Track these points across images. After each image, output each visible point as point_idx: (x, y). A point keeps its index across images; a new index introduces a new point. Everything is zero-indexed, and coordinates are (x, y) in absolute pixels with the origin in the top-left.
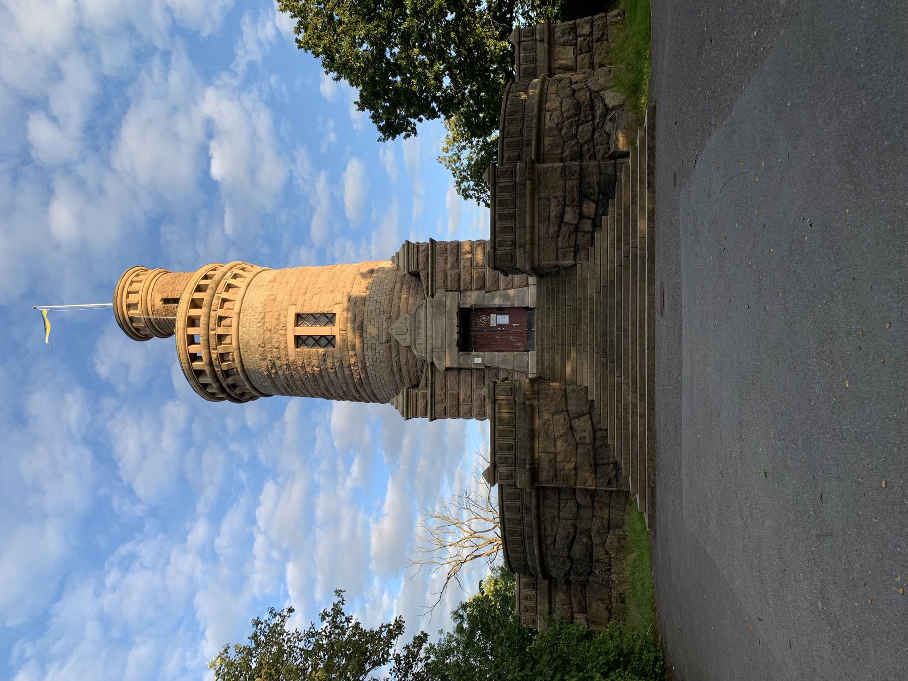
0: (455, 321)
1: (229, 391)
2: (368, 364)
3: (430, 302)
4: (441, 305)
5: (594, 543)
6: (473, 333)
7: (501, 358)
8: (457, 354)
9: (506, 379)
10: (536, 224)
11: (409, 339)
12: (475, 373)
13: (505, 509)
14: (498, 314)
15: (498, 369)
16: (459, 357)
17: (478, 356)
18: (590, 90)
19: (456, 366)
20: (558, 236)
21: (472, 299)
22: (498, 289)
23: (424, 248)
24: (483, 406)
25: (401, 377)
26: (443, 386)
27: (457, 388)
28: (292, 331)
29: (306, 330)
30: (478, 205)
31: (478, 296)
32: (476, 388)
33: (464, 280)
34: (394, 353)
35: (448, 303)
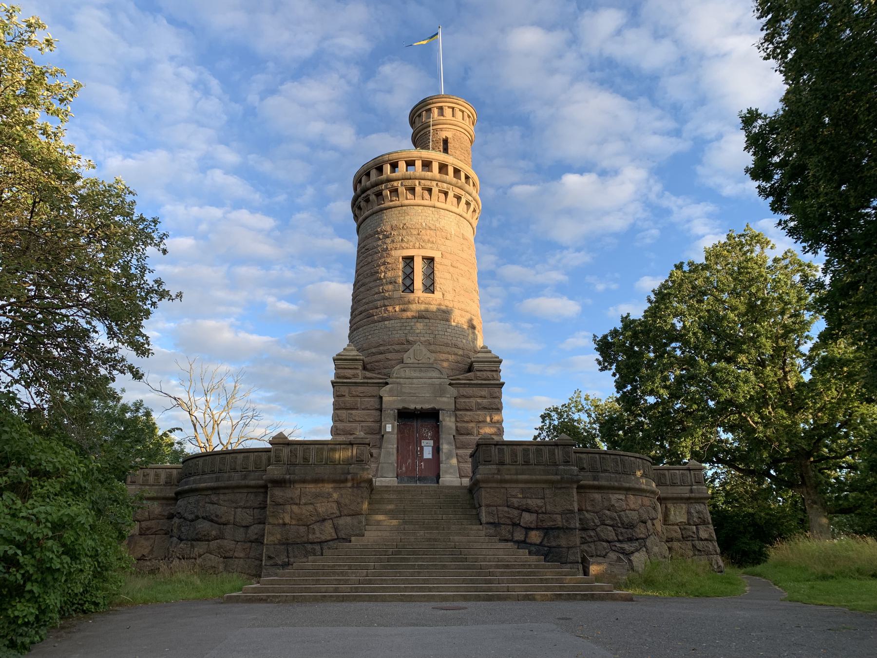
0: (427, 406)
1: (363, 196)
2: (386, 323)
4: (441, 392)
5: (211, 543)
12: (376, 425)
13: (246, 454)
15: (380, 448)
18: (647, 538)
20: (508, 506)
21: (448, 422)
23: (495, 376)
25: (374, 354)
27: (363, 407)
28: (418, 254)
29: (419, 267)
34: (397, 347)
35: (445, 399)
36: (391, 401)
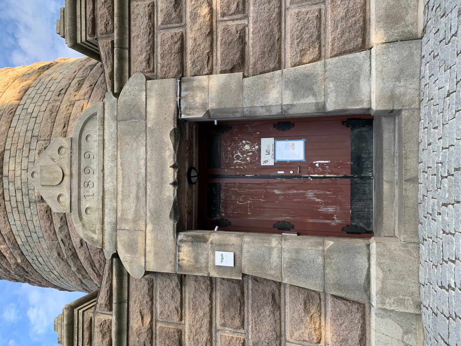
3: (112, 105)
6: (223, 182)
7: (286, 256)
8: (172, 238)
11: (67, 195)
14: (278, 138)
16: (178, 248)
17: (223, 247)
19: (168, 269)
22: (279, 66)
26: (146, 311)
31: (224, 87)
32: (224, 325)
33: (194, 52)
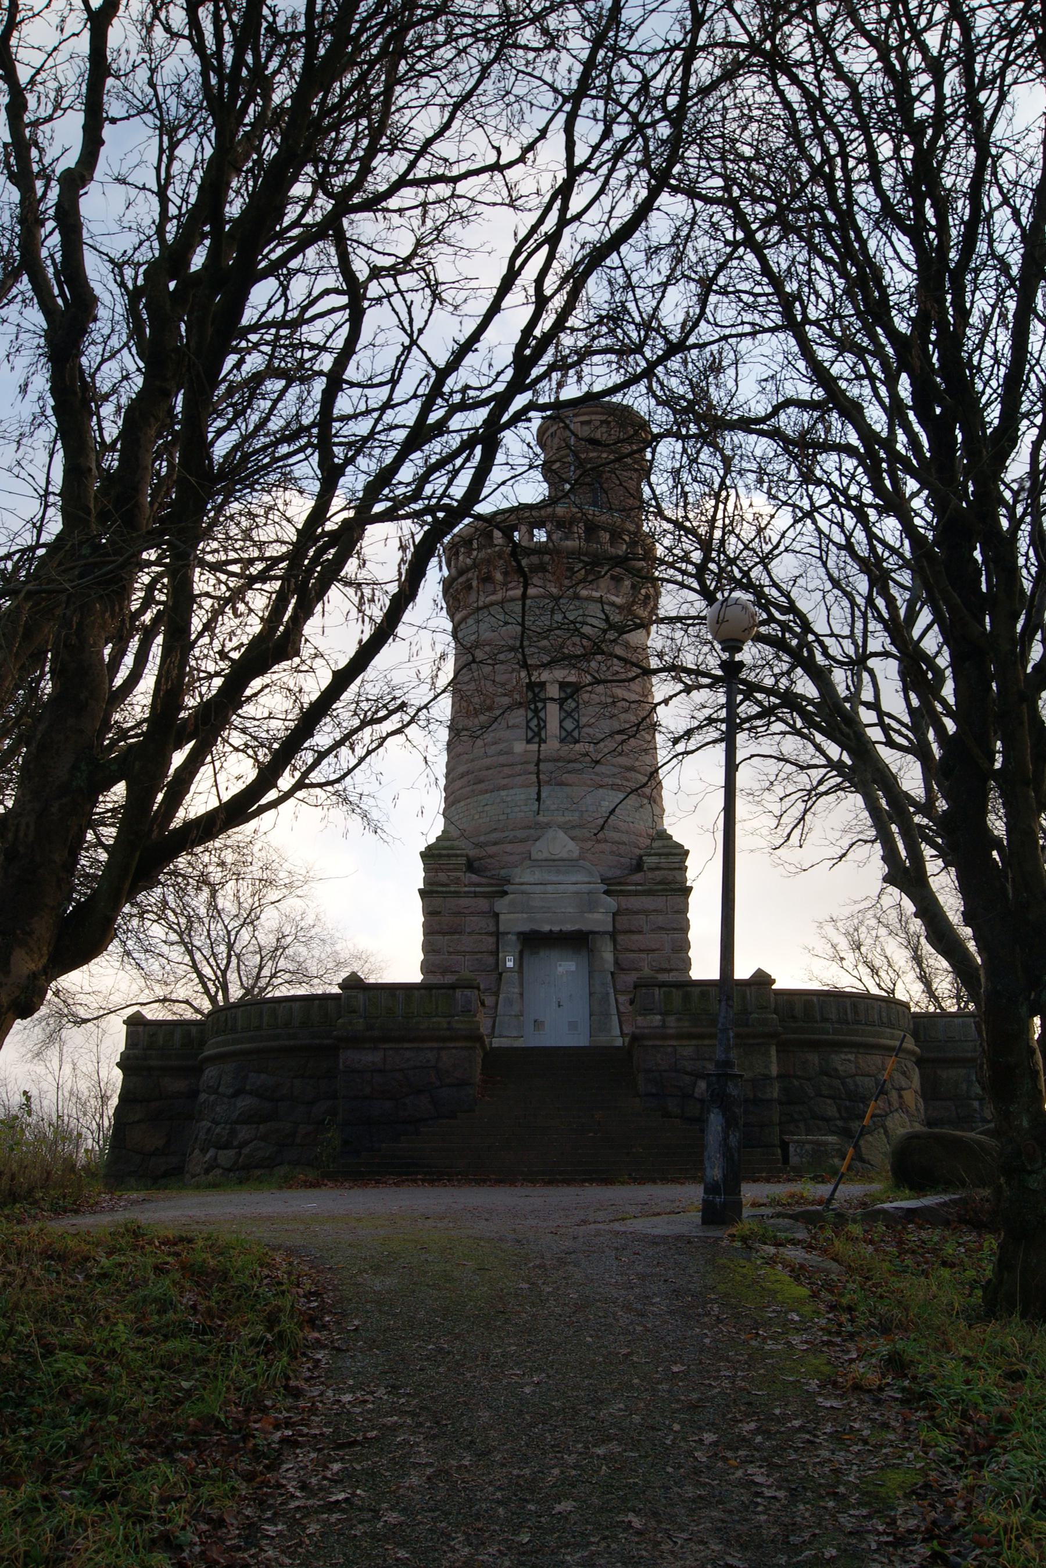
0: (568, 927)
1: (460, 580)
2: (503, 793)
4: (590, 904)
9: (483, 1004)
10: (694, 1042)
15: (497, 994)
18: (886, 1115)
24: (445, 971)
30: (806, 948)
34: (520, 834)
35: (596, 916)
36: (513, 921)
